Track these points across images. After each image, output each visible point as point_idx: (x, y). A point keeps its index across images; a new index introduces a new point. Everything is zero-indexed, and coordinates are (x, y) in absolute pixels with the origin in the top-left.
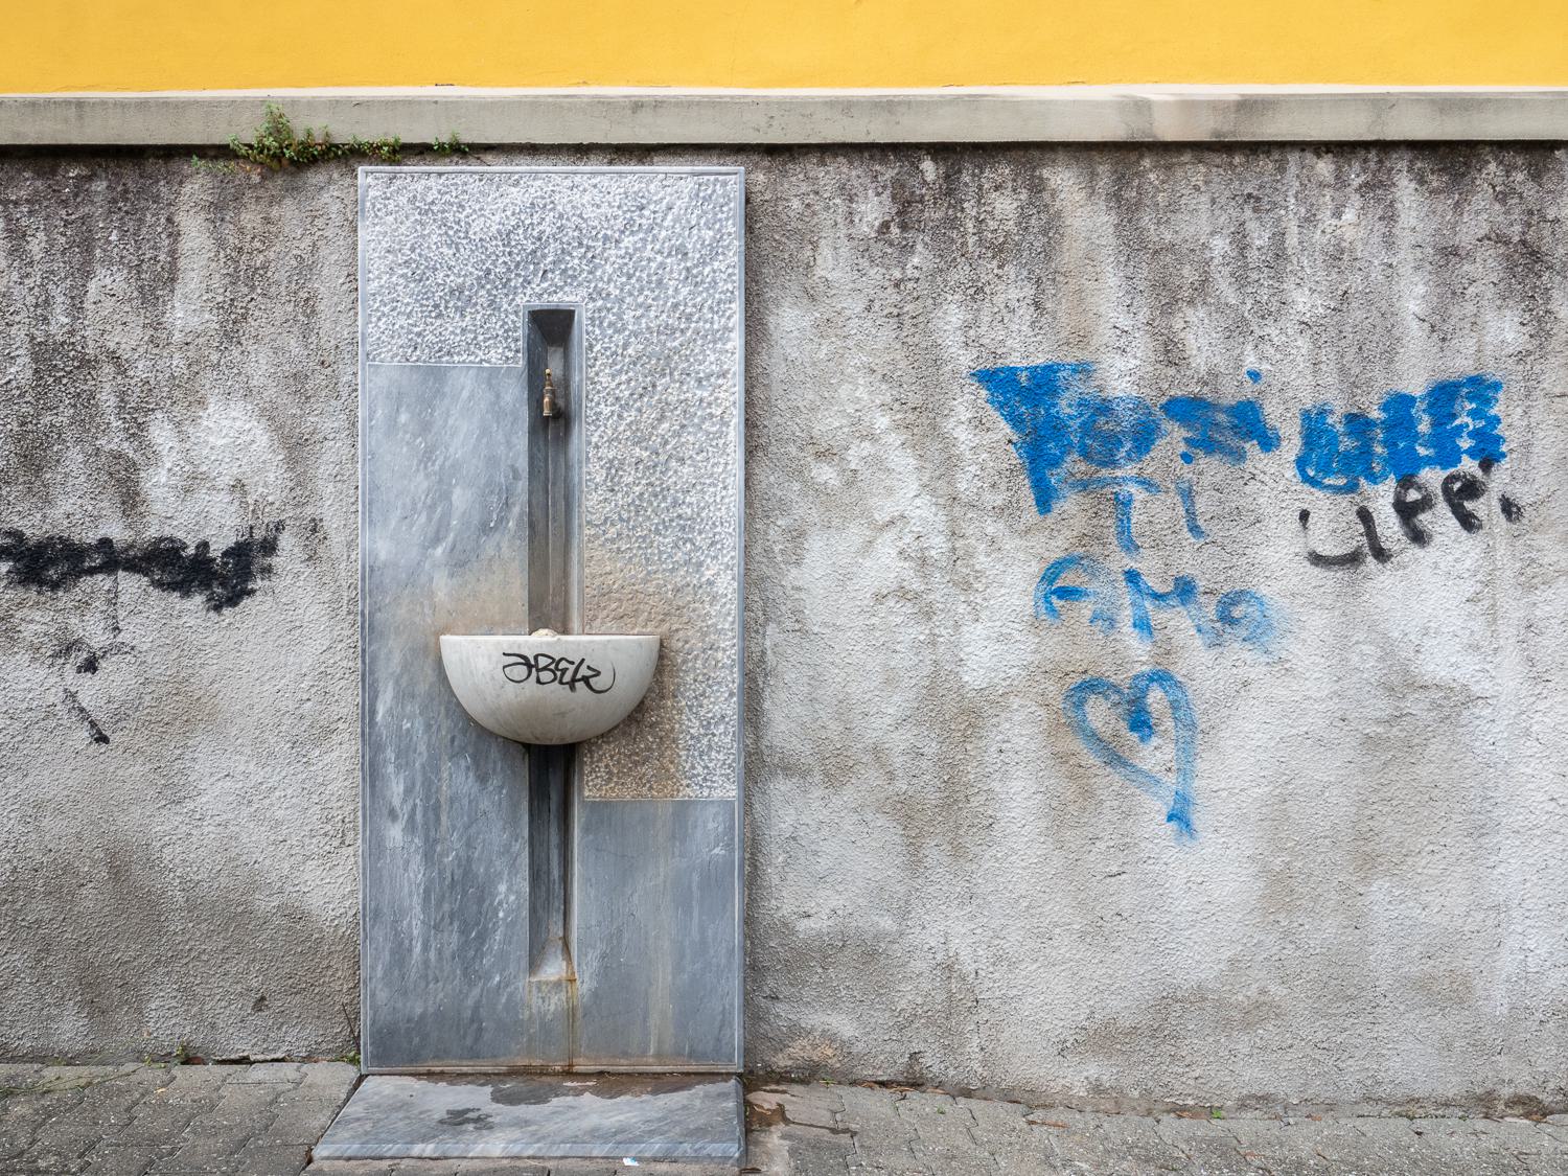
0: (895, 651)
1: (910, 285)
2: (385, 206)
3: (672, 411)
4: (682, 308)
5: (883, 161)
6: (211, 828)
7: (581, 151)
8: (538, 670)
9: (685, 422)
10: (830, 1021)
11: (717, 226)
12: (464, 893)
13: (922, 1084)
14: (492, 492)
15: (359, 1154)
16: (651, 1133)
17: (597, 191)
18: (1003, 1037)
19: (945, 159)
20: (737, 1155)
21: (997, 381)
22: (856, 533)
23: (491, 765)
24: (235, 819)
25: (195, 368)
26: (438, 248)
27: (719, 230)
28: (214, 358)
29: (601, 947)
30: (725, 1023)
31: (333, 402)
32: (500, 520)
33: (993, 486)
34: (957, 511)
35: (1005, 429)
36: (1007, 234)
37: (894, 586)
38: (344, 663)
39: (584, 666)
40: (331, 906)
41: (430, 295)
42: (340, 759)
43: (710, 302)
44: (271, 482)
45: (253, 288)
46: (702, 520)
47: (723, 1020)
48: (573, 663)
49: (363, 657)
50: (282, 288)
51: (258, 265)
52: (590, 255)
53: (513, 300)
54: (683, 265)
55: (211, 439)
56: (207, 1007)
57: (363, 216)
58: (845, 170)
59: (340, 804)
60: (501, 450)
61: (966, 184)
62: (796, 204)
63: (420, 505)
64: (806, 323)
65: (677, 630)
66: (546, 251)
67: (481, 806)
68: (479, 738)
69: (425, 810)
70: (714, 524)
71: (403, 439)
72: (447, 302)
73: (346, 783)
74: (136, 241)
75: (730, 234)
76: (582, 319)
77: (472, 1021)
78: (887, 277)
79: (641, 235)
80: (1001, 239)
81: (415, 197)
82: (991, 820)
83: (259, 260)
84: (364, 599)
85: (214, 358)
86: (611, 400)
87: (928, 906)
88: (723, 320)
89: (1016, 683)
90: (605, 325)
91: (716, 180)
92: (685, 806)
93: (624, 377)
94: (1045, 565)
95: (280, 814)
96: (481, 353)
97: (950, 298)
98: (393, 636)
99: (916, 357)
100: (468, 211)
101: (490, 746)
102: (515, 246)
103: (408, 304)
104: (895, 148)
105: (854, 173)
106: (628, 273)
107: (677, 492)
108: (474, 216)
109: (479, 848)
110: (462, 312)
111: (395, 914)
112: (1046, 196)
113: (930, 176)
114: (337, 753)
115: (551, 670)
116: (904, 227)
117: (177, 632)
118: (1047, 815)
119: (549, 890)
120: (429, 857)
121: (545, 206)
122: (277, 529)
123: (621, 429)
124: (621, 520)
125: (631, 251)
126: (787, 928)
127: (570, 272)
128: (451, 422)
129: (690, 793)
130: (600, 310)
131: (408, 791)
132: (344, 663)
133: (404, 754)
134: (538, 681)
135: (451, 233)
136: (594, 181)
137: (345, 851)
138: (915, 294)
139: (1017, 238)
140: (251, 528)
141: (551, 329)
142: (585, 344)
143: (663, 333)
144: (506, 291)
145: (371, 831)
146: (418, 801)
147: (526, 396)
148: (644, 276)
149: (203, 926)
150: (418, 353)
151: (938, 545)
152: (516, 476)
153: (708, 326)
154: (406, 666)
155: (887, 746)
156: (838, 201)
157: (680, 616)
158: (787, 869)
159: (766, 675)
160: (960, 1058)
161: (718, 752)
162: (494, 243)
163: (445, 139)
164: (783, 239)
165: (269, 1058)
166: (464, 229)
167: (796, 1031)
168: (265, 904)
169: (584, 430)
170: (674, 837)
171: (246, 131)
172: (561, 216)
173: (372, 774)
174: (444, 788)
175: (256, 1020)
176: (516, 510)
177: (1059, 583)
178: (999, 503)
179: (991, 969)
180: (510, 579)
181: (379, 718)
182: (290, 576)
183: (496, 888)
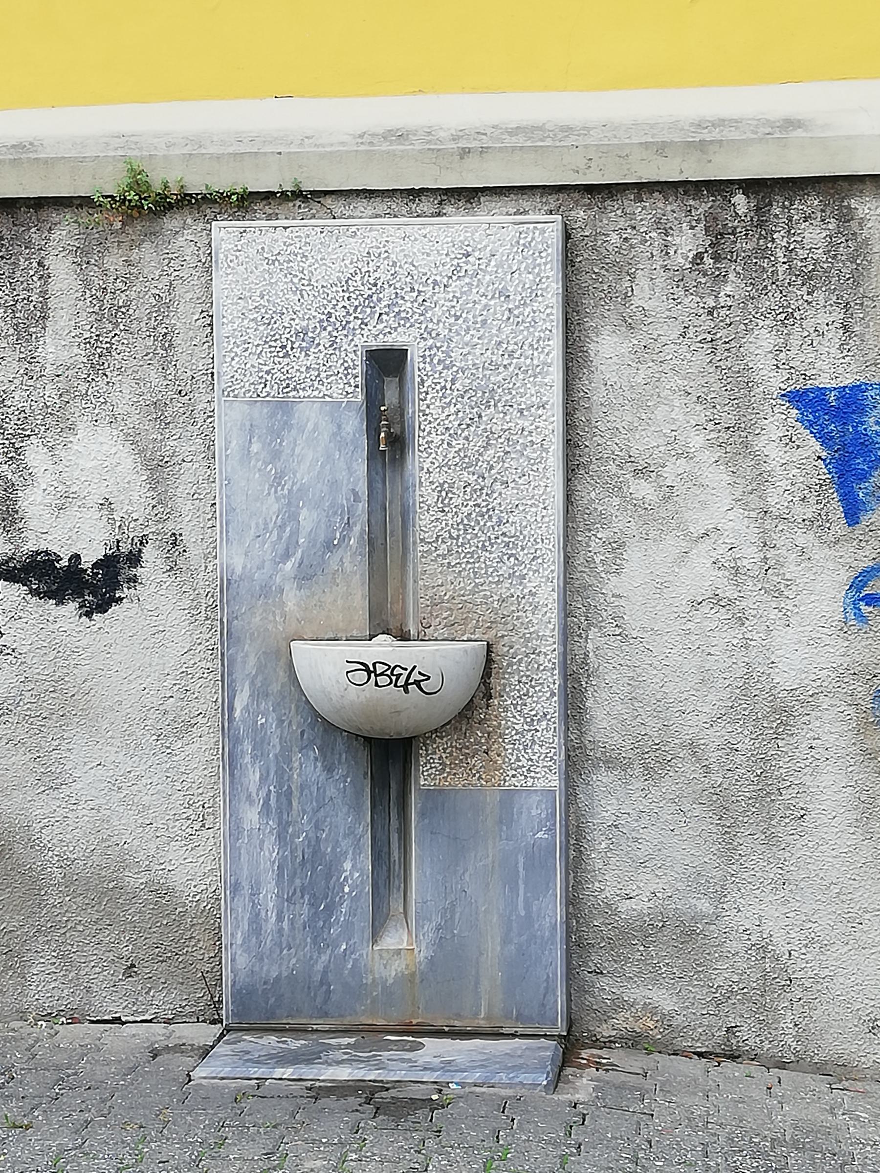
0: (709, 654)
1: (723, 312)
2: (237, 257)
3: (496, 439)
4: (505, 346)
5: (697, 196)
6: (85, 812)
7: (414, 194)
8: (376, 676)
9: (508, 449)
10: (643, 994)
11: (536, 271)
12: (313, 870)
13: (738, 1057)
14: (335, 513)
15: (231, 1076)
16: (474, 1067)
17: (422, 242)
18: (816, 1014)
19: (756, 193)
20: (545, 1083)
21: (807, 401)
22: (672, 544)
23: (337, 756)
24: (106, 804)
25: (65, 398)
26: (284, 294)
27: (538, 274)
28: (83, 388)
29: (437, 919)
30: (549, 989)
31: (190, 428)
32: (343, 538)
33: (803, 500)
34: (769, 524)
35: (814, 446)
36: (816, 262)
37: (709, 594)
38: (203, 664)
39: (416, 670)
40: (194, 883)
41: (277, 337)
42: (200, 751)
43: (530, 340)
44: (135, 501)
45: (117, 325)
46: (524, 537)
47: (547, 988)
48: (406, 669)
49: (222, 660)
50: (143, 324)
51: (121, 304)
52: (420, 299)
53: (352, 340)
54: (506, 306)
55: (81, 462)
56: (83, 973)
57: (217, 267)
58: (661, 205)
59: (200, 791)
60: (342, 475)
61: (776, 216)
62: (614, 238)
63: (271, 525)
64: (625, 349)
65: (503, 636)
66: (381, 296)
67: (328, 793)
68: (326, 731)
69: (279, 795)
70: (535, 540)
71: (255, 466)
72: (293, 343)
73: (206, 772)
74: (11, 283)
75: (548, 278)
76: (414, 357)
77: (322, 983)
78: (702, 305)
79: (467, 280)
80: (811, 267)
81: (263, 248)
82: (802, 812)
83: (121, 300)
84: (222, 609)
85: (83, 388)
86: (441, 429)
87: (743, 891)
88: (542, 356)
89: (825, 684)
90: (435, 361)
91: (535, 228)
92: (510, 794)
93: (453, 409)
94: (853, 574)
95: (146, 800)
96: (324, 389)
97: (761, 323)
98: (249, 641)
99: (729, 380)
100: (311, 260)
101: (335, 740)
102: (353, 292)
103: (258, 345)
104: (709, 185)
105: (669, 208)
106: (455, 315)
107: (502, 512)
108: (317, 265)
109: (327, 830)
110: (306, 351)
111: (252, 889)
112: (854, 224)
113: (742, 210)
114: (198, 745)
115: (387, 675)
116: (717, 258)
117: (54, 635)
118: (856, 808)
119: (388, 871)
120: (281, 838)
121: (380, 255)
122: (141, 543)
123: (450, 456)
124: (451, 537)
125: (458, 295)
126: (609, 909)
127: (403, 315)
128: (297, 450)
129: (518, 782)
130: (430, 349)
131: (263, 779)
132: (203, 664)
133: (260, 745)
134: (377, 684)
135: (296, 280)
136: (424, 232)
137: (205, 833)
138: (728, 321)
139: (825, 266)
140: (118, 542)
141: (386, 364)
142: (417, 379)
143: (487, 369)
144: (345, 332)
145: (231, 815)
146: (272, 788)
147: (365, 427)
148: (470, 317)
149: (78, 899)
150: (268, 389)
151: (750, 556)
152: (357, 499)
153: (528, 361)
154: (261, 668)
155: (702, 742)
156: (653, 234)
157: (506, 624)
158: (609, 854)
159: (589, 675)
160: (774, 1033)
161: (541, 746)
162: (334, 289)
163: (288, 187)
164: (603, 272)
165: (139, 1019)
166: (307, 278)
167: (619, 1004)
168: (134, 880)
169: (417, 457)
170: (501, 822)
171: (109, 182)
172: (394, 264)
173: (232, 763)
174: (295, 776)
175: (128, 984)
176: (357, 529)
177: (867, 591)
178: (809, 515)
179: (803, 951)
180: (351, 595)
181: (237, 714)
182: (154, 585)
183: (342, 866)
